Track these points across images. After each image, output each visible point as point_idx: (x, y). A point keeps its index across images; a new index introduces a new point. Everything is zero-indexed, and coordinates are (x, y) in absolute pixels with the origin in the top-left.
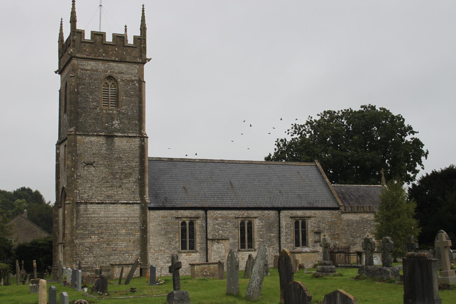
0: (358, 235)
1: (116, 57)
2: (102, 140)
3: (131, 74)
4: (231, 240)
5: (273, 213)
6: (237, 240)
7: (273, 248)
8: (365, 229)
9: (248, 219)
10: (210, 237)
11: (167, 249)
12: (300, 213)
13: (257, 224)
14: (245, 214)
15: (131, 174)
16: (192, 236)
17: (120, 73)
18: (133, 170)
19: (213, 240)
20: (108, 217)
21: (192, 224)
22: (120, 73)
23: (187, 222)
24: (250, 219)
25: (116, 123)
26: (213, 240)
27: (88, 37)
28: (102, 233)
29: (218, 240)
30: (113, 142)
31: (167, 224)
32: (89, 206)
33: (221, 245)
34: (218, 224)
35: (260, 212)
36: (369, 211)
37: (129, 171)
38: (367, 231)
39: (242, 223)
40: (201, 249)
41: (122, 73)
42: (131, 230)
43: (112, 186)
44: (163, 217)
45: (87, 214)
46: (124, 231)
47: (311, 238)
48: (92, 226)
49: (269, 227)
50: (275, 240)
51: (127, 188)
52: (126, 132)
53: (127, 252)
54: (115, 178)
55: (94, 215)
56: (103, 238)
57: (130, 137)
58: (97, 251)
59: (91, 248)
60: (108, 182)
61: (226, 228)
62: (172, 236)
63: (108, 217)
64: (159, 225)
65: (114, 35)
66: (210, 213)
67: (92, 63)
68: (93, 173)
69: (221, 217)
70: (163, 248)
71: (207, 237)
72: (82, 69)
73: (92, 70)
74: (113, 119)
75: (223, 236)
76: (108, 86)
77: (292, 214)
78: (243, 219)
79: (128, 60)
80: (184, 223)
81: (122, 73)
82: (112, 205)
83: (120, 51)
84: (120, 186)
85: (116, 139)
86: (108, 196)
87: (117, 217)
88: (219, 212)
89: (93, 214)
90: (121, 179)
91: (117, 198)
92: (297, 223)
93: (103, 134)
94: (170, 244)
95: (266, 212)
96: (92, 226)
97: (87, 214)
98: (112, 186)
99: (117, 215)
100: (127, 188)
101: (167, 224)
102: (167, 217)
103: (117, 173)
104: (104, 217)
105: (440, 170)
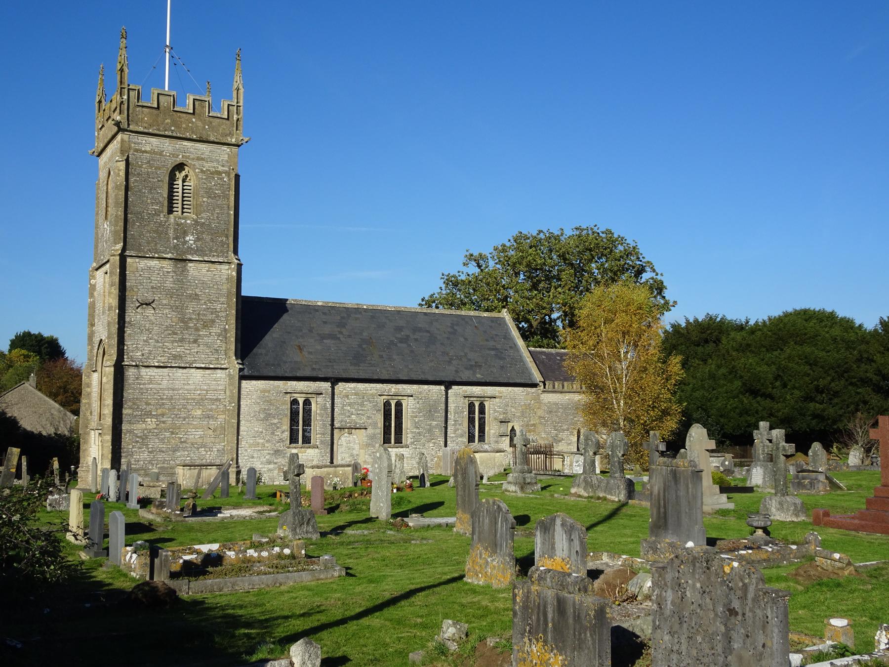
0: (565, 427)
2: (168, 266)
3: (218, 161)
4: (370, 431)
6: (378, 431)
7: (434, 443)
11: (268, 441)
12: (477, 390)
13: (408, 406)
16: (307, 422)
18: (218, 316)
20: (173, 390)
21: (307, 402)
22: (199, 159)
25: (190, 238)
28: (163, 415)
32: (144, 371)
33: (351, 438)
35: (415, 387)
39: (387, 405)
40: (322, 442)
41: (203, 159)
42: (211, 410)
43: (182, 340)
44: (264, 391)
46: (199, 412)
47: (491, 429)
48: (148, 404)
49: (429, 411)
51: (207, 345)
53: (204, 446)
54: (188, 328)
56: (164, 422)
58: (154, 443)
59: (144, 437)
60: (176, 334)
62: (276, 421)
63: (173, 390)
64: (258, 403)
66: (341, 387)
67: (154, 140)
69: (356, 394)
71: (332, 425)
72: (137, 150)
73: (152, 152)
74: (185, 233)
75: (356, 423)
77: (466, 391)
81: (203, 159)
83: (200, 124)
84: (195, 341)
85: (190, 265)
88: (352, 385)
89: (149, 384)
90: (197, 330)
92: (471, 406)
94: (273, 433)
96: (148, 404)
100: (207, 345)
102: (269, 391)
103: (191, 319)
104: (168, 389)
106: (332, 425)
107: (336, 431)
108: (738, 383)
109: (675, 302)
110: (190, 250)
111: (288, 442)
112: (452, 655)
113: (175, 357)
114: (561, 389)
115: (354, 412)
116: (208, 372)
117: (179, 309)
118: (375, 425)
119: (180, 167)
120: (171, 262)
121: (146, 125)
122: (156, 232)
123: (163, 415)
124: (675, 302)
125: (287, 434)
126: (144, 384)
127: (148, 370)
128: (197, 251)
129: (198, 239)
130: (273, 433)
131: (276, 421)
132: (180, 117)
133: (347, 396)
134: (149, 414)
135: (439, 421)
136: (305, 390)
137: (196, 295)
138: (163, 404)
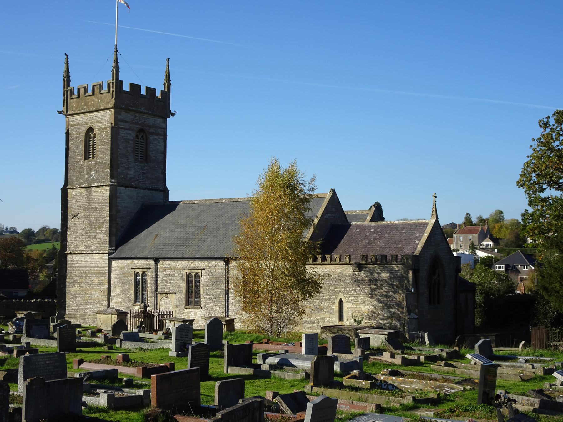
0: (327, 297)
1: (94, 106)
2: (83, 190)
4: (178, 295)
5: (221, 264)
8: (336, 288)
9: (194, 271)
10: (159, 291)
13: (204, 276)
14: (192, 265)
15: (103, 223)
17: (98, 122)
19: (161, 293)
20: (86, 267)
22: (98, 122)
23: (141, 273)
24: (196, 271)
26: (161, 293)
27: (143, 92)
28: (82, 282)
29: (167, 294)
30: (91, 193)
31: (124, 274)
32: (74, 256)
33: (167, 300)
34: (167, 276)
35: (206, 262)
36: (348, 262)
37: (102, 221)
38: (340, 291)
42: (102, 280)
43: (89, 237)
44: (122, 268)
45: (73, 264)
48: (76, 276)
50: (222, 298)
52: (100, 182)
53: (99, 302)
55: (77, 265)
56: (82, 287)
57: (102, 186)
58: (78, 299)
60: (87, 233)
61: (174, 280)
62: (127, 287)
63: (86, 267)
65: (131, 84)
66: (162, 264)
68: (77, 224)
70: (120, 300)
74: (91, 170)
76: (138, 138)
78: (190, 271)
79: (102, 108)
80: (136, 275)
82: (89, 255)
85: (93, 189)
86: (87, 247)
87: (92, 267)
89: (77, 264)
90: (96, 230)
91: (93, 248)
93: (84, 185)
95: (213, 262)
96: (76, 276)
97: (73, 264)
98: (89, 237)
99: (92, 265)
101: (124, 274)
102: (124, 268)
105: (258, 188)
106: (156, 290)
107: (159, 295)
108: (532, 408)
109: (467, 214)
110: (93, 181)
111: (133, 302)
112: (535, 241)
113: (87, 247)
114: (348, 262)
115: (169, 282)
116: (101, 255)
117: (88, 217)
118: (181, 293)
119: (91, 129)
120: (85, 189)
121: (74, 109)
122: (79, 172)
123: (82, 282)
124: (467, 214)
125: (132, 297)
126: (74, 264)
127: (75, 255)
128: (97, 180)
129: (97, 173)
130: (126, 295)
131: (127, 287)
132: (88, 99)
133: (165, 270)
134: (76, 282)
135: (222, 290)
136: (142, 266)
137: (96, 208)
138: (82, 276)
